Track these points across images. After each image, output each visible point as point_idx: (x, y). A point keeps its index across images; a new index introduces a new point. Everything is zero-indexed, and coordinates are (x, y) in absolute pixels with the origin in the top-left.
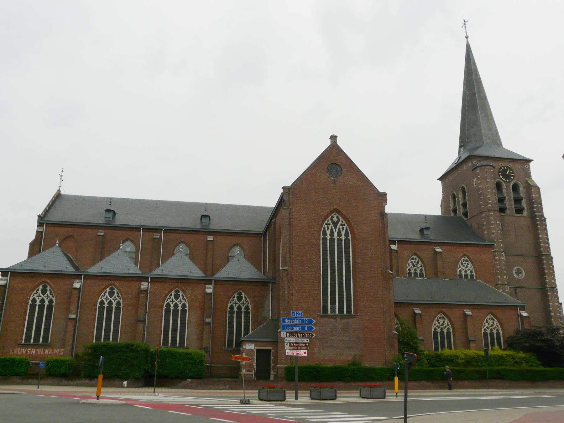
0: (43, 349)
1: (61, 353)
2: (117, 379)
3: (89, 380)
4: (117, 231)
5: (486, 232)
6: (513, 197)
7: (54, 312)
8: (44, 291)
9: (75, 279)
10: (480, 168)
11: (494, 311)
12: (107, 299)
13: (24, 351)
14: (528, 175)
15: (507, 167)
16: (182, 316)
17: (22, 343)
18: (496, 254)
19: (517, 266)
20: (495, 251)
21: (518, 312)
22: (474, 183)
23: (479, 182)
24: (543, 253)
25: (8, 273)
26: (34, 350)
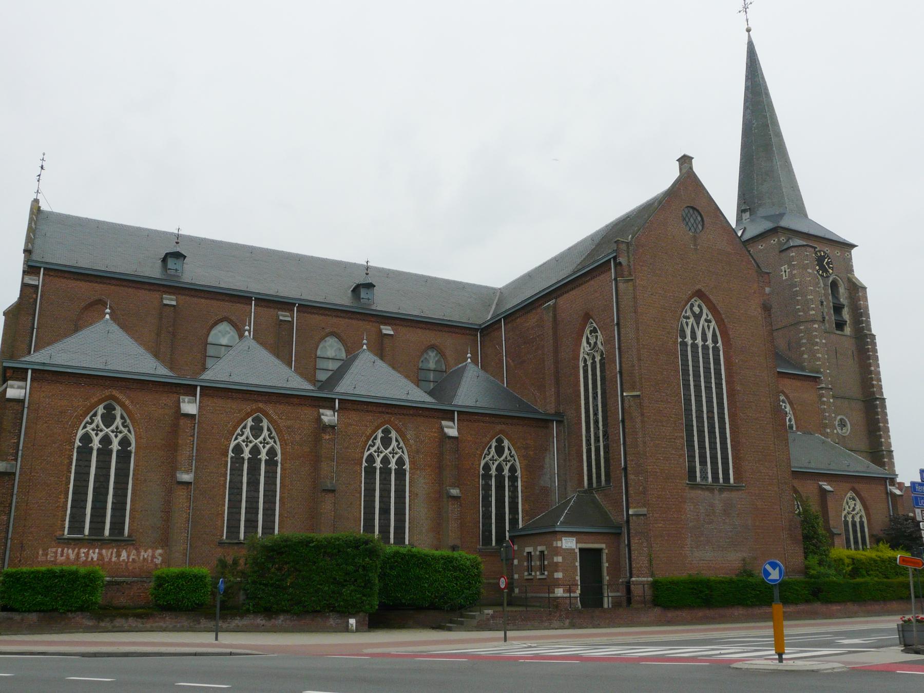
0: (115, 550)
1: (156, 558)
2: (331, 614)
3: (264, 617)
4: (203, 300)
5: (806, 356)
6: (833, 303)
7: (136, 465)
8: (108, 419)
9: (179, 394)
10: (796, 249)
11: (856, 486)
12: (247, 442)
13: (71, 553)
14: (850, 269)
15: (824, 252)
16: (398, 482)
17: (63, 534)
18: (823, 393)
19: (844, 415)
20: (822, 388)
21: (886, 487)
22: (783, 273)
23: (795, 272)
24: (878, 396)
25: (27, 372)
26: (94, 553)
